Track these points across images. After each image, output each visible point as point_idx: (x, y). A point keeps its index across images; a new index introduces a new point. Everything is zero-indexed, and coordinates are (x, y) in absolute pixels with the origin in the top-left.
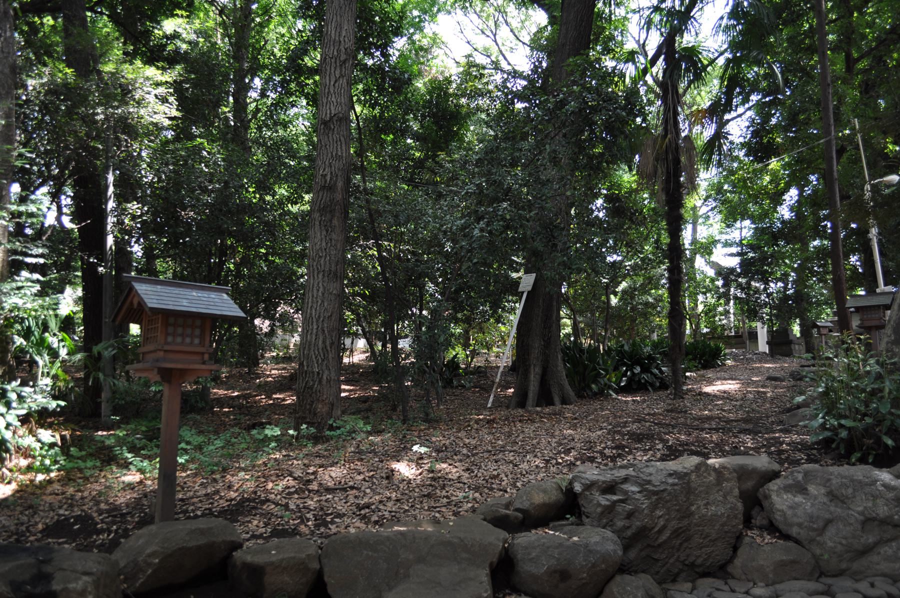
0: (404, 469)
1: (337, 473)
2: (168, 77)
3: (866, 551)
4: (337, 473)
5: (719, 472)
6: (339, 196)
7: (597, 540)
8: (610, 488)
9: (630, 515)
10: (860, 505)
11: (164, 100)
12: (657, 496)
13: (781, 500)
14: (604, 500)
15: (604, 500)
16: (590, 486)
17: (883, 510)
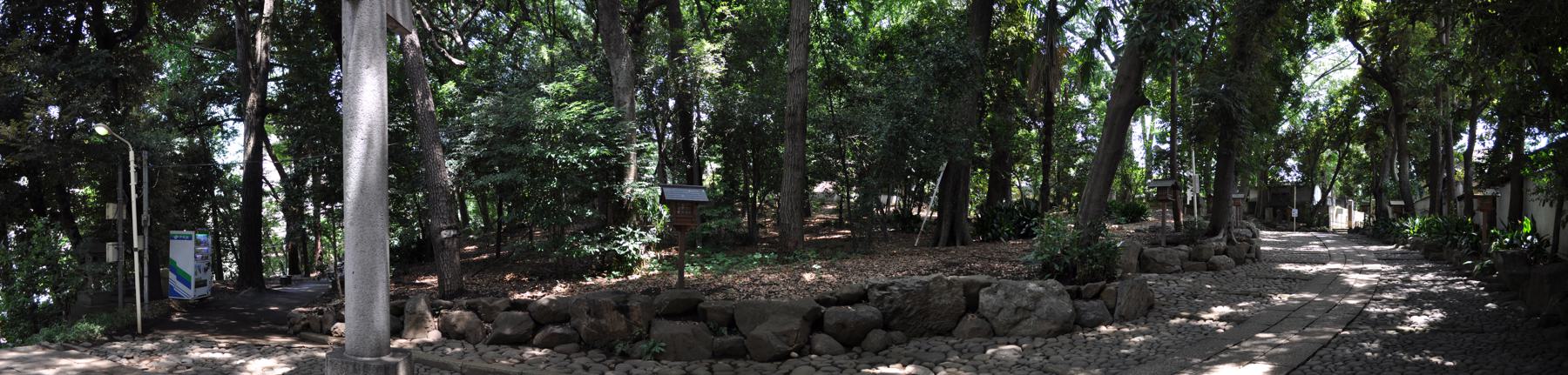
0: (808, 277)
1: (772, 277)
2: (718, 46)
3: (1017, 323)
4: (772, 277)
5: (950, 283)
6: (798, 119)
7: (866, 311)
8: (883, 287)
9: (891, 301)
10: (1016, 301)
11: (717, 61)
12: (907, 293)
13: (984, 298)
14: (878, 293)
15: (878, 293)
16: (872, 286)
17: (1025, 303)
